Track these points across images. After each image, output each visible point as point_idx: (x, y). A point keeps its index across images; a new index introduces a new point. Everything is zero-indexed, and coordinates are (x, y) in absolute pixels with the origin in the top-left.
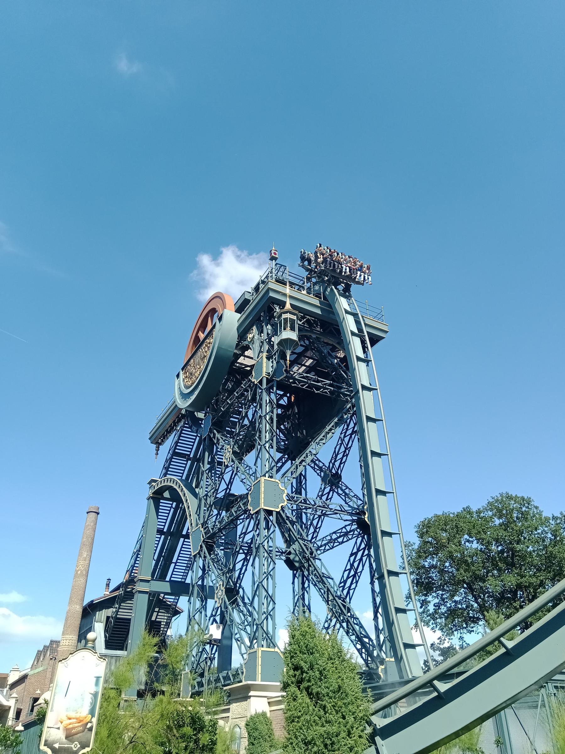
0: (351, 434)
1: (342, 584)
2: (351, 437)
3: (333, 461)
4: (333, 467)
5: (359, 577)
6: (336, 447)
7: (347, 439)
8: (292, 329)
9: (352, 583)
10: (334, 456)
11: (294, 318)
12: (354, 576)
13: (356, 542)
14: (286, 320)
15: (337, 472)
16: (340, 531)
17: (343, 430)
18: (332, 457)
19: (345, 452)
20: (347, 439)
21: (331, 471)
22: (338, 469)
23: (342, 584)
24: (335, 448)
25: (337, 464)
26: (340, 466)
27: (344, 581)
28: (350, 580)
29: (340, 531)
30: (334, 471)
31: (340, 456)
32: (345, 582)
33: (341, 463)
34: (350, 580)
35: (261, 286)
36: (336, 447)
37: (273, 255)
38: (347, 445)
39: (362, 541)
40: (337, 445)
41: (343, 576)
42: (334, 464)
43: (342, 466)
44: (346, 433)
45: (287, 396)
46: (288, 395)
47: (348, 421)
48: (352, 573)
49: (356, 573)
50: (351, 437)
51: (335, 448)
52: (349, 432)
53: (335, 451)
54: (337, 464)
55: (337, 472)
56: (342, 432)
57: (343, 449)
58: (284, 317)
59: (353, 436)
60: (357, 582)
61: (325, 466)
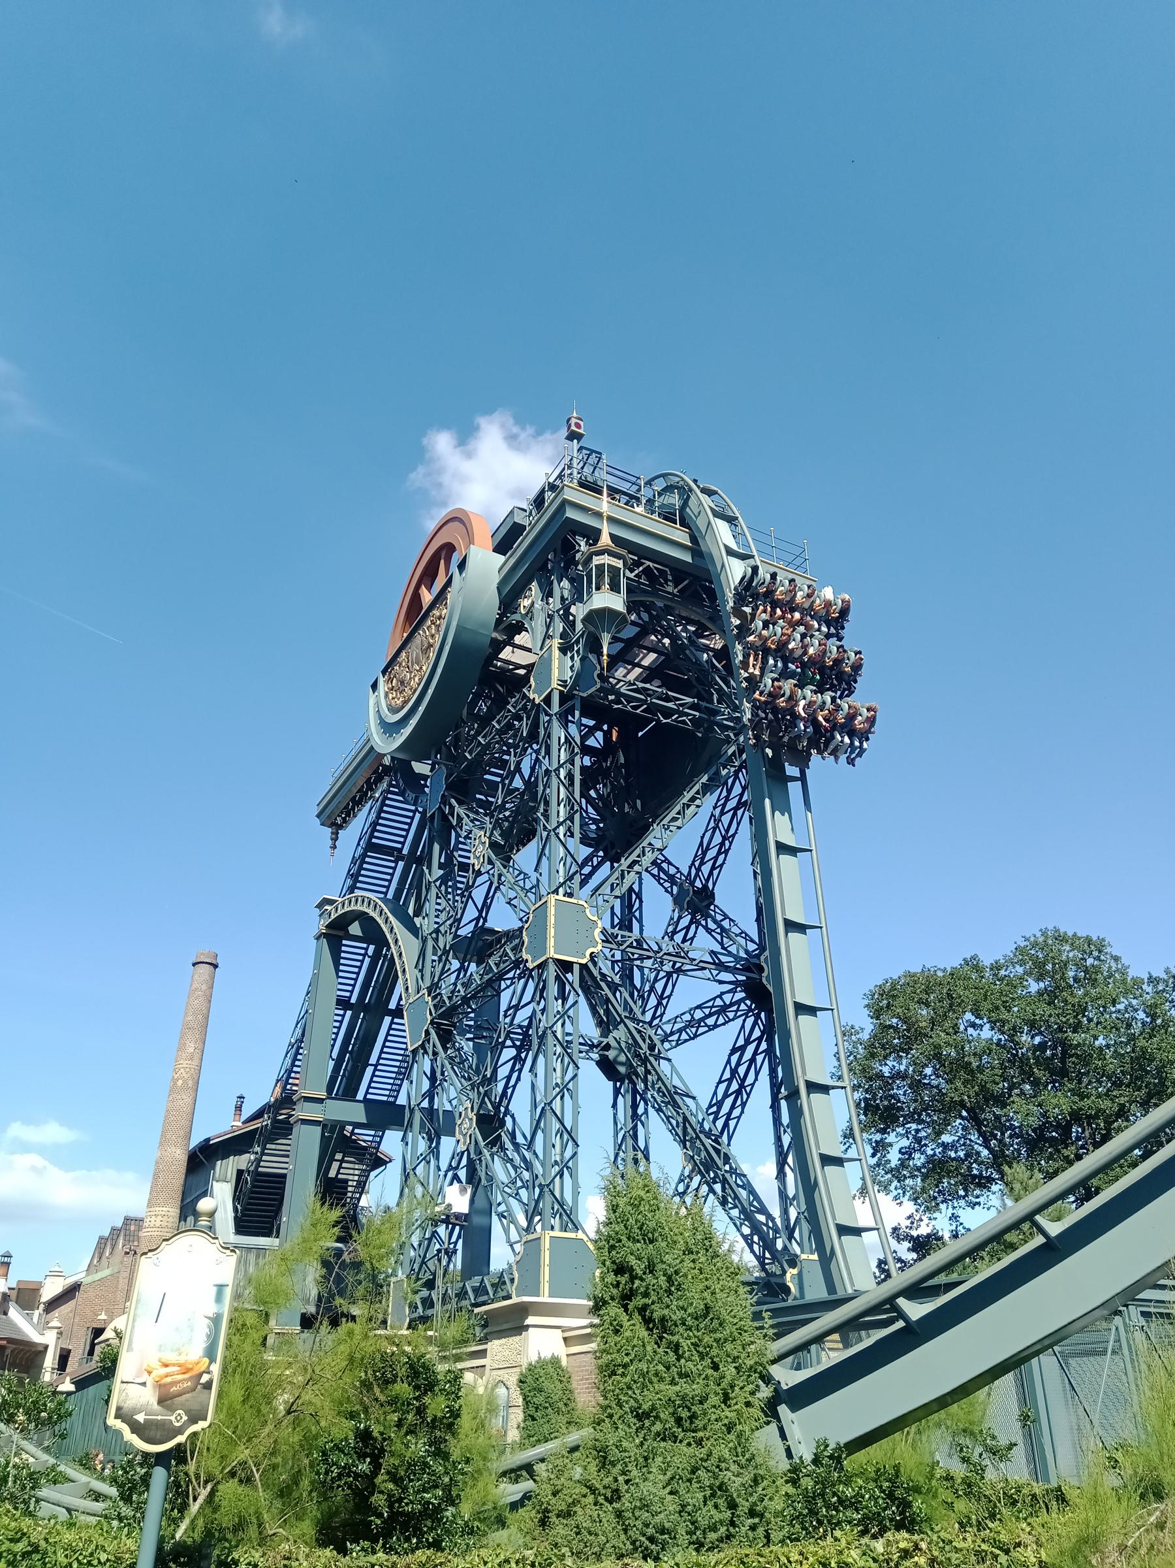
0: (736, 809)
1: (714, 1109)
2: (735, 814)
3: (697, 864)
4: (697, 875)
5: (748, 1095)
6: (704, 834)
7: (726, 819)
8: (615, 588)
9: (733, 1107)
10: (700, 852)
11: (618, 566)
12: (738, 1093)
13: (743, 1026)
14: (600, 568)
15: (705, 887)
16: (710, 1004)
17: (718, 800)
18: (696, 856)
19: (722, 844)
20: (726, 819)
21: (692, 883)
22: (707, 880)
23: (714, 1109)
24: (702, 838)
25: (706, 869)
26: (711, 873)
27: (718, 1102)
28: (728, 1102)
29: (710, 1004)
30: (698, 884)
31: (711, 853)
32: (720, 1104)
33: (713, 868)
34: (728, 1102)
35: (549, 496)
36: (704, 834)
37: (573, 428)
38: (727, 831)
39: (755, 1024)
40: (706, 831)
41: (715, 1093)
42: (698, 870)
43: (716, 872)
44: (724, 805)
45: (602, 730)
46: (605, 727)
47: (730, 781)
48: (735, 1086)
49: (742, 1086)
50: (735, 814)
51: (702, 838)
52: (732, 804)
53: (701, 844)
54: (706, 869)
55: (705, 887)
56: (716, 804)
57: (718, 839)
58: (598, 563)
59: (740, 813)
60: (744, 1105)
61: (681, 874)
